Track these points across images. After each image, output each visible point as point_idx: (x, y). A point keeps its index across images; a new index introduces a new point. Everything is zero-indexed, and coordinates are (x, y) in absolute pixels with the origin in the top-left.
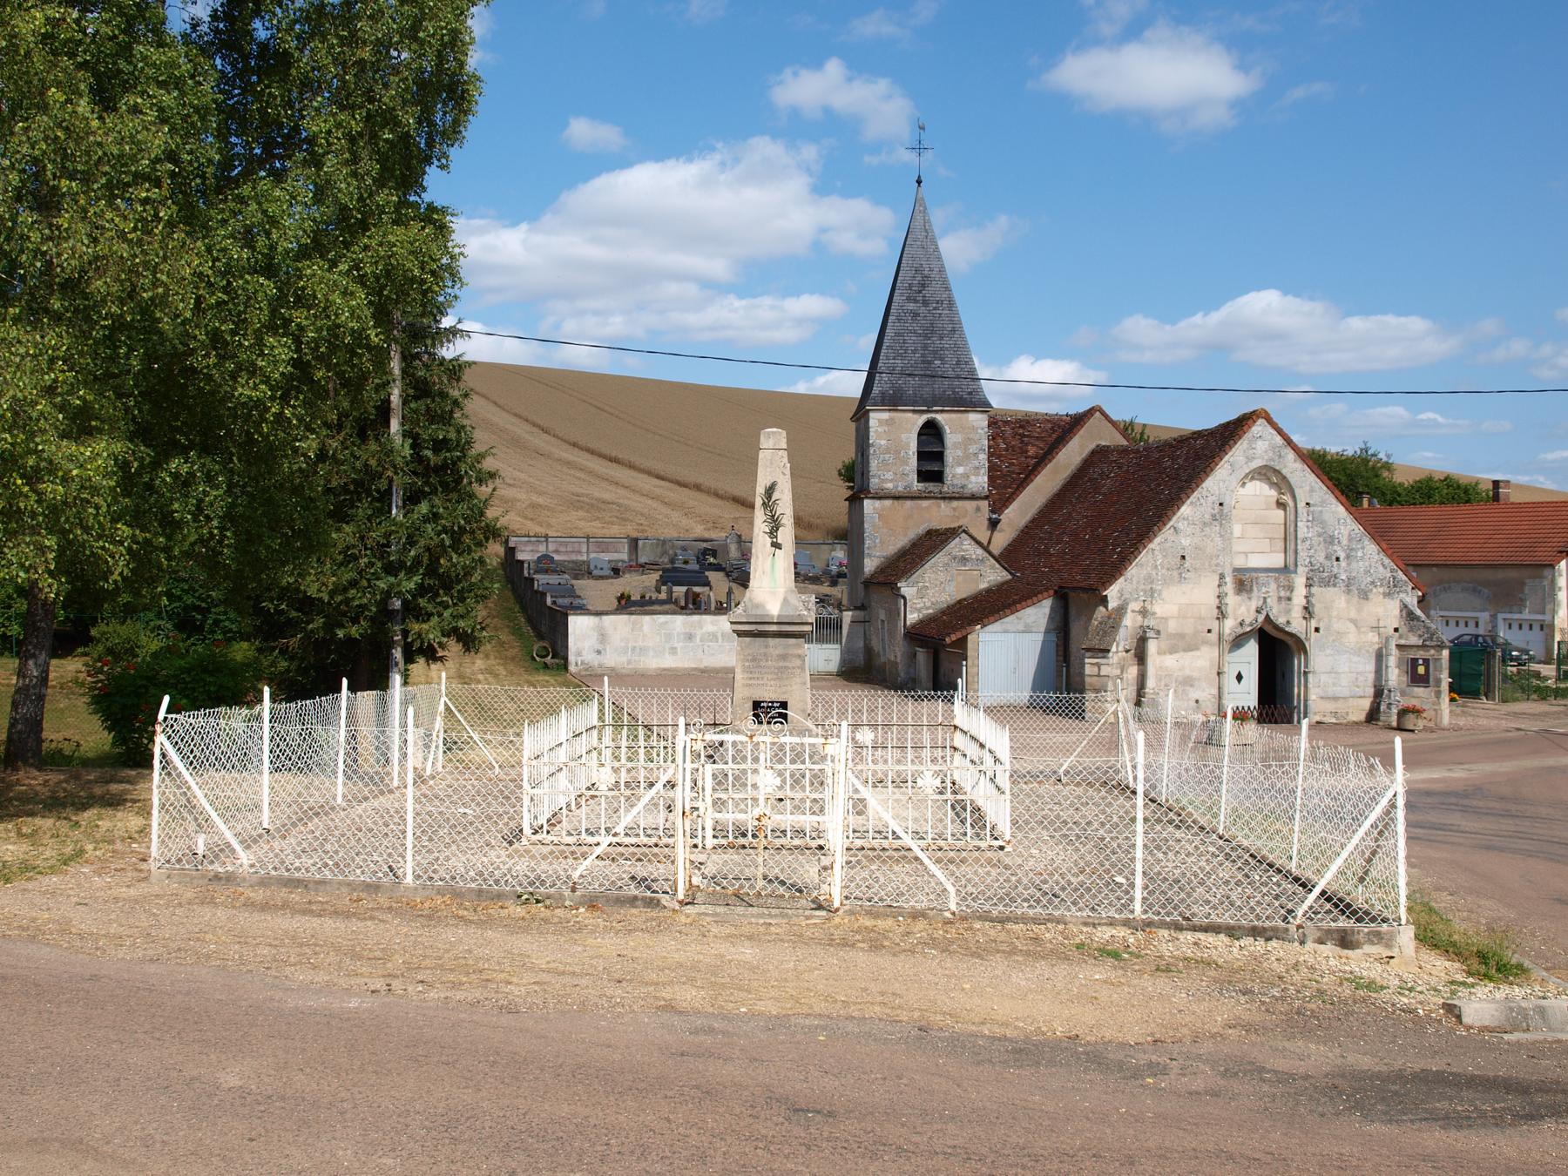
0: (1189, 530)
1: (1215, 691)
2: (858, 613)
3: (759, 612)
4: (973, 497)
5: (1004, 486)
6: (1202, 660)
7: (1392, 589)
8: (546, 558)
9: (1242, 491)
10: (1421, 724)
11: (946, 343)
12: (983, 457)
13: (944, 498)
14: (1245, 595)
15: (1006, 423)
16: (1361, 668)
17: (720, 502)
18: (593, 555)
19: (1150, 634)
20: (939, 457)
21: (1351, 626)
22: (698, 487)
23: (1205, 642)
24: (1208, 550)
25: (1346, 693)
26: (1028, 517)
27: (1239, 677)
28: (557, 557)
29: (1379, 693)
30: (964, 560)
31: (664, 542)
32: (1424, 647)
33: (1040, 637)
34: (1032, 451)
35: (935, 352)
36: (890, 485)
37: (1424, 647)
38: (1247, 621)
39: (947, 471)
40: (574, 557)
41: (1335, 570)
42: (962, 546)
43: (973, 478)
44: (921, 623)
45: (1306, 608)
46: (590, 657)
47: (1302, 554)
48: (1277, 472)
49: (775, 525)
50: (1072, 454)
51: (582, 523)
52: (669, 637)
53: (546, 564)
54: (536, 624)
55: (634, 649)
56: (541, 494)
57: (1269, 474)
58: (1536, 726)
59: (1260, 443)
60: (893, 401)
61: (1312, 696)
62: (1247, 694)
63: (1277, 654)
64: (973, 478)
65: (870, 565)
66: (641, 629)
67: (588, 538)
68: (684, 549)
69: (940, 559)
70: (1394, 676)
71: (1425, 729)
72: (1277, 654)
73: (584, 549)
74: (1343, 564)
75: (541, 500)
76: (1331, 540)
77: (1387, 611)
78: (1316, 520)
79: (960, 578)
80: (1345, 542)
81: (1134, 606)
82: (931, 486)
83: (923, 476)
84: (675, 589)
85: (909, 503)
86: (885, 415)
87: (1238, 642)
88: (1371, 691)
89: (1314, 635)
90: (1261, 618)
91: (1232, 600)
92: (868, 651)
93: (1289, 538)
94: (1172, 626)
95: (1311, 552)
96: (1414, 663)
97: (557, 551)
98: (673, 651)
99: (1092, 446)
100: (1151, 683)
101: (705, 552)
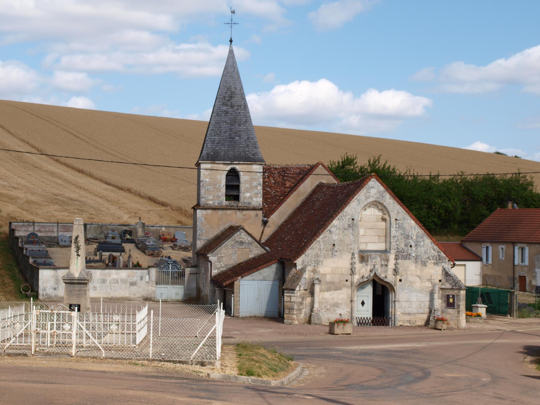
0: (337, 232)
1: (349, 310)
2: (193, 269)
3: (72, 276)
4: (254, 209)
5: (271, 203)
6: (343, 295)
7: (438, 261)
8: (33, 235)
9: (364, 213)
10: (445, 326)
11: (242, 128)
12: (260, 188)
13: (239, 209)
14: (364, 264)
15: (276, 169)
17: (141, 200)
18: (60, 233)
19: (316, 282)
20: (237, 187)
21: (418, 279)
22: (129, 190)
23: (345, 286)
24: (346, 242)
25: (415, 311)
26: (283, 220)
27: (363, 303)
28: (39, 234)
29: (431, 311)
30: (242, 243)
31: (102, 226)
32: (452, 289)
33: (270, 283)
34: (288, 184)
35: (236, 133)
36: (211, 202)
37: (452, 289)
38: (366, 276)
39: (241, 195)
40: (49, 234)
41: (410, 252)
42: (241, 236)
43: (255, 199)
44: (219, 275)
45: (395, 270)
46: (50, 292)
47: (393, 244)
48: (381, 204)
49: (78, 248)
50: (307, 186)
51: (56, 213)
53: (33, 239)
56: (33, 194)
57: (378, 204)
60: (213, 158)
61: (398, 313)
62: (367, 312)
63: (382, 294)
64: (255, 199)
65: (200, 244)
67: (58, 223)
68: (113, 231)
69: (229, 242)
70: (438, 303)
71: (448, 329)
72: (382, 294)
73: (55, 230)
74: (414, 248)
75: (33, 198)
76: (407, 237)
78: (400, 227)
79: (240, 252)
80: (414, 238)
81: (309, 268)
82: (233, 203)
83: (228, 197)
84: (104, 253)
85: (220, 212)
86: (209, 166)
87: (361, 285)
88: (427, 310)
89: (398, 283)
90: (372, 274)
91: (358, 265)
92: (199, 290)
93: (387, 236)
94: (328, 278)
95: (398, 242)
97: (39, 231)
99: (317, 183)
100: (316, 306)
101: (125, 232)
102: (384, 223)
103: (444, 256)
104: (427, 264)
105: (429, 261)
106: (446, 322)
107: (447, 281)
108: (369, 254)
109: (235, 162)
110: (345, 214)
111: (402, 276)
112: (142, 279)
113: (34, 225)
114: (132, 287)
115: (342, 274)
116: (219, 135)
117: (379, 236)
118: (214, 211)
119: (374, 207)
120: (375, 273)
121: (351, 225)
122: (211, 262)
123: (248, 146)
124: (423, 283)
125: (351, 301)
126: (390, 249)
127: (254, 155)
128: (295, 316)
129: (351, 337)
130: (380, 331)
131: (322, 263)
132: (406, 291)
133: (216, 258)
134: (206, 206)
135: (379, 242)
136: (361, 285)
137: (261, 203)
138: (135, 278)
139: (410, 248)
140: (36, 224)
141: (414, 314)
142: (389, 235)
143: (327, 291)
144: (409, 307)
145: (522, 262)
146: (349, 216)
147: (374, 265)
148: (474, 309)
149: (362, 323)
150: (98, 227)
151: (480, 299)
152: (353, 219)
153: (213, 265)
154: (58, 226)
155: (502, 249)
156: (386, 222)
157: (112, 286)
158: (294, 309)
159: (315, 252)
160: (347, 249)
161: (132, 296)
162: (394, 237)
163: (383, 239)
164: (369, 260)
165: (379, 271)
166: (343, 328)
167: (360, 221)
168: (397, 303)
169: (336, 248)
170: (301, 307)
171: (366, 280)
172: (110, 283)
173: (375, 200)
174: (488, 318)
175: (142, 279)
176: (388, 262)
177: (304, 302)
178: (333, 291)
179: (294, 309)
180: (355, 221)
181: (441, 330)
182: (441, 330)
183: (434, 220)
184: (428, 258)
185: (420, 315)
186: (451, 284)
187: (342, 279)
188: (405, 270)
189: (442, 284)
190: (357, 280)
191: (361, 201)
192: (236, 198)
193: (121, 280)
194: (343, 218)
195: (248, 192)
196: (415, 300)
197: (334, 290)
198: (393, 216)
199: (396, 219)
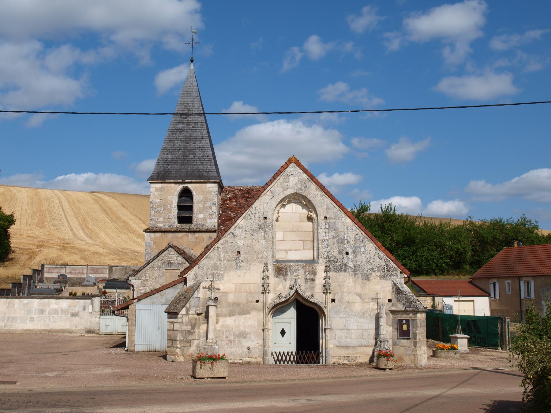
0: (243, 235)
1: (261, 342)
4: (207, 231)
6: (252, 321)
7: (386, 273)
10: (390, 365)
13: (190, 232)
14: (282, 278)
15: (240, 191)
20: (190, 208)
21: (358, 298)
23: (254, 309)
25: (355, 343)
27: (283, 333)
28: (69, 276)
30: (170, 263)
32: (405, 312)
35: (191, 150)
36: (161, 225)
37: (405, 312)
38: (284, 295)
39: (194, 216)
40: (79, 276)
41: (345, 261)
43: (209, 220)
45: (324, 286)
47: (322, 250)
48: (305, 197)
52: (29, 312)
55: (9, 318)
62: (289, 344)
63: (309, 320)
64: (209, 220)
66: (13, 307)
70: (388, 331)
72: (309, 320)
73: (85, 271)
74: (351, 256)
76: (342, 241)
77: (383, 288)
78: (331, 228)
79: (168, 275)
80: (352, 242)
82: (185, 226)
83: (181, 220)
87: (278, 309)
89: (330, 305)
91: (273, 280)
94: (231, 298)
97: (70, 273)
98: (32, 319)
100: (211, 336)
103: (395, 266)
104: (371, 278)
105: (373, 274)
106: (391, 358)
107: (399, 300)
108: (289, 264)
109: (186, 181)
111: (335, 294)
112: (84, 309)
113: (66, 268)
114: (74, 318)
115: (250, 293)
116: (172, 154)
117: (304, 241)
119: (296, 203)
120: (297, 291)
122: (133, 286)
123: (202, 163)
125: (263, 330)
126: (318, 258)
127: (208, 172)
128: (178, 350)
129: (225, 383)
130: (307, 372)
132: (341, 315)
134: (155, 229)
135: (304, 249)
136: (278, 309)
137: (216, 224)
138: (77, 308)
139: (345, 256)
140: (67, 267)
141: (354, 347)
143: (230, 316)
144: (346, 337)
145: (528, 296)
147: (296, 279)
148: (452, 340)
149: (280, 359)
150: (123, 269)
151: (459, 328)
152: (265, 218)
153: (135, 289)
154: (87, 268)
155: (509, 283)
156: (313, 222)
157: (51, 317)
158: (176, 340)
159: (212, 262)
160: (257, 258)
161: (74, 328)
162: (323, 241)
164: (289, 273)
165: (302, 288)
166: (211, 369)
167: (277, 220)
170: (190, 338)
171: (283, 300)
172: (49, 314)
173: (295, 191)
174: (471, 352)
175: (84, 309)
176: (315, 274)
177: (196, 331)
178: (238, 316)
179: (176, 340)
181: (385, 369)
182: (385, 369)
183: (446, 261)
184: (372, 269)
185: (362, 348)
186: (404, 304)
187: (250, 299)
188: (339, 286)
189: (393, 305)
190: (272, 300)
193: (62, 311)
194: (252, 216)
197: (240, 314)
199: (325, 217)
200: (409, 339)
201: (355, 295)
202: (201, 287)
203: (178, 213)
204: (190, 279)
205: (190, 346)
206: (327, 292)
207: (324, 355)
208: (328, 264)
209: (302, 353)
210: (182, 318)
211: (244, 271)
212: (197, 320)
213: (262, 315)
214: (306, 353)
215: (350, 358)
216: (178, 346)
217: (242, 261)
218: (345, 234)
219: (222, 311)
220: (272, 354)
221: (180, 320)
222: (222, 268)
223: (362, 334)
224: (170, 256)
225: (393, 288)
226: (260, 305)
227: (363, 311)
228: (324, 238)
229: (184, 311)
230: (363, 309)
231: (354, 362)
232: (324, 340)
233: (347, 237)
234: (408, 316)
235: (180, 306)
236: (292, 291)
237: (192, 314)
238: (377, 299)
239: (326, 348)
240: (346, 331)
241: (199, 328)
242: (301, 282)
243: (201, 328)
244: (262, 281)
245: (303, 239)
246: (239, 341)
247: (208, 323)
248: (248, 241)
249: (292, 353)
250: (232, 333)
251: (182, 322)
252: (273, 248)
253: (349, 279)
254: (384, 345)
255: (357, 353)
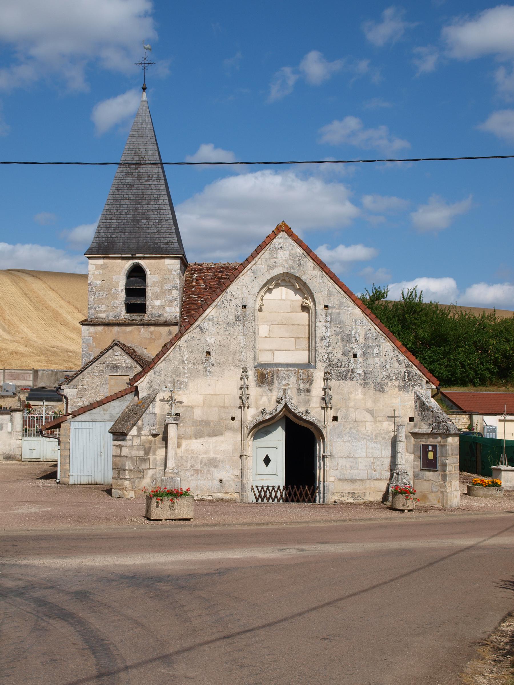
0: (214, 329)
1: (238, 472)
4: (166, 324)
6: (226, 444)
7: (407, 382)
10: (410, 504)
12: (176, 294)
13: (143, 325)
15: (210, 269)
16: (377, 453)
20: (142, 293)
21: (368, 416)
23: (229, 428)
24: (231, 347)
25: (363, 475)
27: (267, 461)
30: (116, 367)
32: (432, 435)
35: (143, 213)
36: (103, 315)
37: (432, 435)
38: (268, 410)
39: (148, 304)
41: (352, 365)
43: (168, 309)
45: (323, 399)
47: (321, 351)
48: (298, 279)
54: (126, 441)
58: (321, 462)
59: (281, 253)
61: (331, 478)
62: (276, 476)
64: (168, 309)
70: (408, 460)
72: (303, 444)
74: (360, 359)
76: (348, 339)
77: (402, 402)
78: (333, 321)
79: (113, 382)
80: (361, 340)
82: (136, 316)
83: (131, 308)
85: (116, 328)
87: (261, 429)
89: (331, 424)
90: (280, 407)
91: (254, 391)
93: (312, 336)
94: (198, 414)
96: (425, 448)
100: (171, 464)
102: (306, 315)
103: (419, 373)
104: (387, 389)
105: (390, 384)
108: (275, 369)
109: (137, 255)
110: (229, 297)
111: (337, 410)
115: (224, 407)
116: (117, 217)
118: (106, 328)
119: (286, 286)
120: (286, 406)
121: (241, 318)
122: (66, 398)
123: (159, 231)
124: (378, 424)
126: (316, 361)
127: (167, 244)
128: (127, 483)
129: (189, 526)
130: (298, 513)
131: (186, 386)
132: (346, 438)
133: (75, 391)
134: (96, 321)
136: (261, 429)
137: (178, 315)
139: (352, 359)
141: (361, 480)
142: (313, 336)
143: (196, 438)
144: (351, 468)
146: (237, 301)
147: (285, 390)
148: (494, 473)
149: (263, 495)
150: (52, 374)
151: (504, 457)
152: (245, 307)
154: (4, 373)
156: (309, 313)
158: (125, 470)
159: (172, 366)
160: (234, 361)
162: (323, 338)
163: (305, 343)
164: (275, 381)
166: (171, 508)
167: (260, 310)
168: (327, 460)
169: (212, 359)
170: (143, 466)
171: (268, 417)
173: (285, 271)
176: (311, 384)
177: (151, 457)
178: (206, 438)
179: (125, 470)
180: (249, 310)
181: (402, 511)
182: (402, 511)
183: (489, 366)
184: (388, 377)
186: (430, 425)
187: (223, 415)
189: (415, 426)
190: (253, 417)
191: (259, 273)
192: (141, 308)
194: (226, 303)
195: (158, 299)
196: (364, 454)
197: (209, 436)
198: (321, 299)
199: (326, 307)
200: (437, 471)
201: (365, 412)
202: (157, 399)
203: (126, 300)
204: (142, 389)
205: (143, 477)
206: (327, 407)
207: (322, 491)
208: (329, 369)
209: (293, 488)
210: (132, 440)
211: (215, 378)
212: (153, 444)
213: (239, 437)
214: (298, 488)
215: (357, 495)
216: (127, 477)
217: (213, 365)
218: (353, 329)
219: (185, 432)
220: (252, 488)
221: (129, 443)
222: (185, 373)
223: (373, 463)
224: (116, 357)
225: (415, 402)
226: (236, 423)
227: (375, 433)
228: (325, 334)
229: (134, 431)
230: (375, 430)
231: (362, 501)
232: (322, 471)
233: (355, 333)
234: (436, 440)
235: (129, 424)
236: (279, 405)
237: (145, 435)
238: (394, 417)
239: (324, 482)
240: (351, 459)
241: (154, 454)
242: (292, 393)
243: (157, 453)
244: (240, 392)
245: (295, 336)
246: (209, 471)
247: (166, 447)
248: (220, 338)
249: (279, 488)
250: (199, 461)
251: (132, 446)
252: (254, 348)
253: (357, 390)
254: (402, 479)
255: (365, 489)
